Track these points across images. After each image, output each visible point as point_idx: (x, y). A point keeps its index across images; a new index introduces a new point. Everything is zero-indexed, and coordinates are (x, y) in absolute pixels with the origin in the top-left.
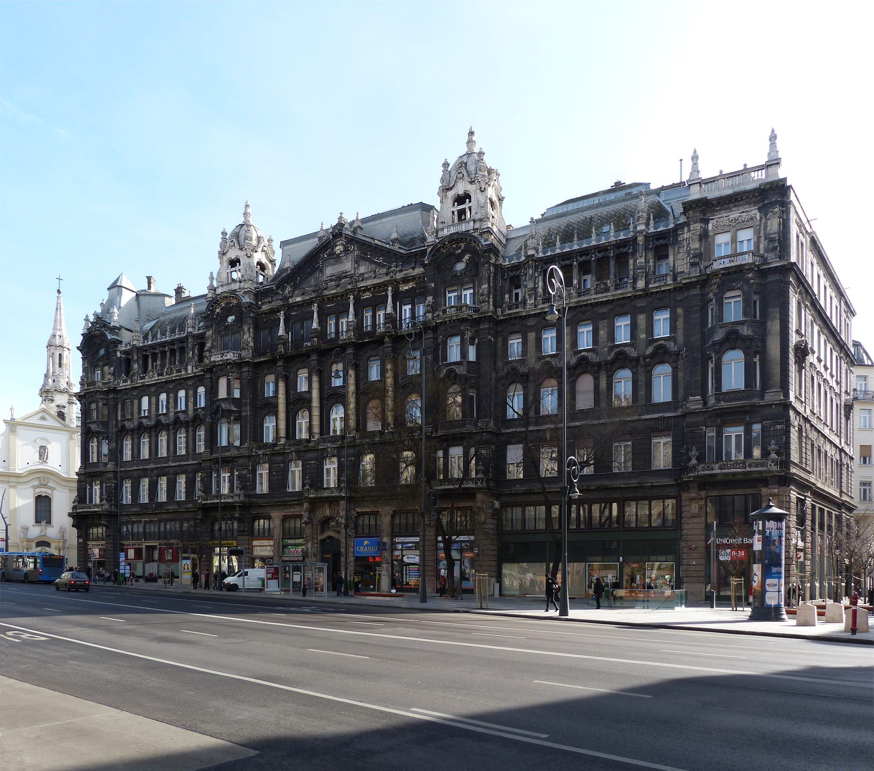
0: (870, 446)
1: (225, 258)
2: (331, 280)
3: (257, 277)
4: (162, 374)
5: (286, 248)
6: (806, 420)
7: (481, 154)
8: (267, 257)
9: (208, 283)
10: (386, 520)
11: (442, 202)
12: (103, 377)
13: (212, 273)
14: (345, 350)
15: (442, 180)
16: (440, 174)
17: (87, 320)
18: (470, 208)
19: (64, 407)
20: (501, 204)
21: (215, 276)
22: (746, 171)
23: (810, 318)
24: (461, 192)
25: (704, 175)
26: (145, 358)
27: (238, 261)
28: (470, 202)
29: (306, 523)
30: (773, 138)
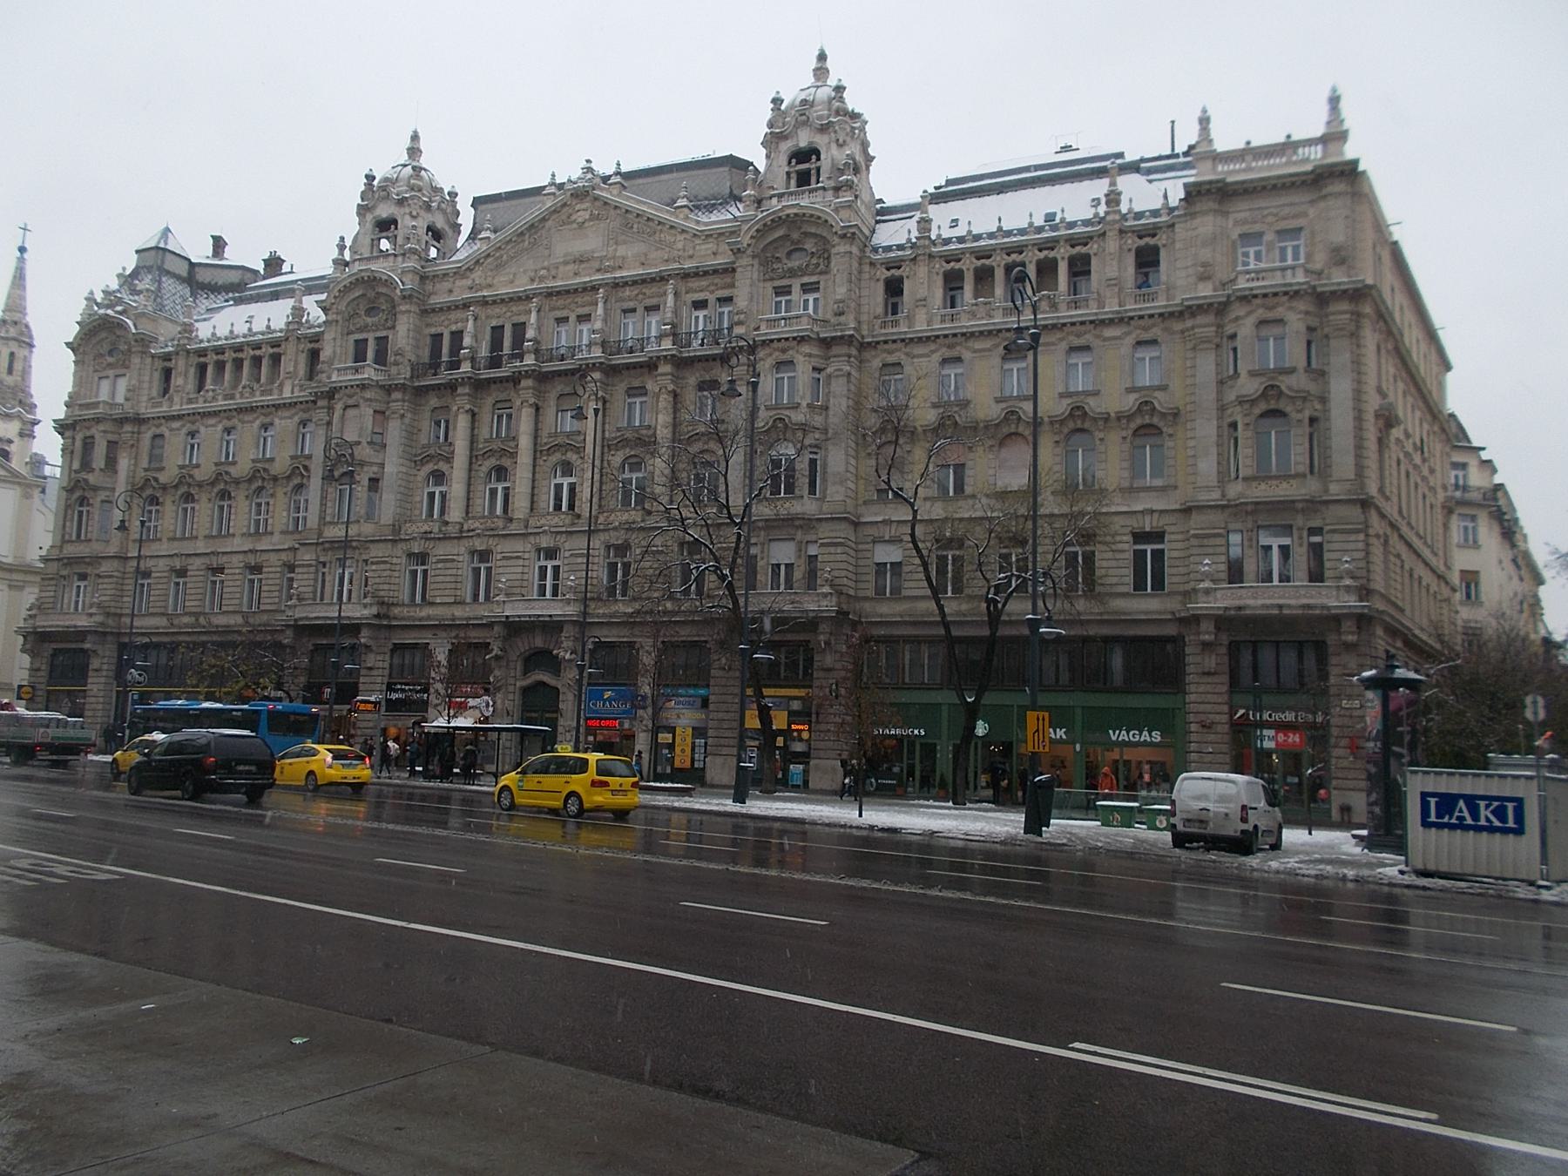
0: (1477, 573)
1: (369, 217)
2: (566, 263)
3: (427, 250)
4: (232, 397)
5: (481, 208)
6: (1393, 526)
7: (839, 89)
8: (448, 221)
9: (335, 254)
10: (441, 656)
11: (768, 157)
12: (115, 392)
13: (342, 239)
14: (656, 367)
15: (771, 125)
16: (769, 115)
17: (90, 299)
18: (818, 170)
19: (10, 442)
20: (868, 168)
21: (348, 243)
22: (1289, 146)
23: (1392, 370)
24: (803, 144)
25: (1221, 144)
26: (202, 369)
27: (395, 222)
28: (818, 159)
29: (497, 658)
30: (1334, 101)
